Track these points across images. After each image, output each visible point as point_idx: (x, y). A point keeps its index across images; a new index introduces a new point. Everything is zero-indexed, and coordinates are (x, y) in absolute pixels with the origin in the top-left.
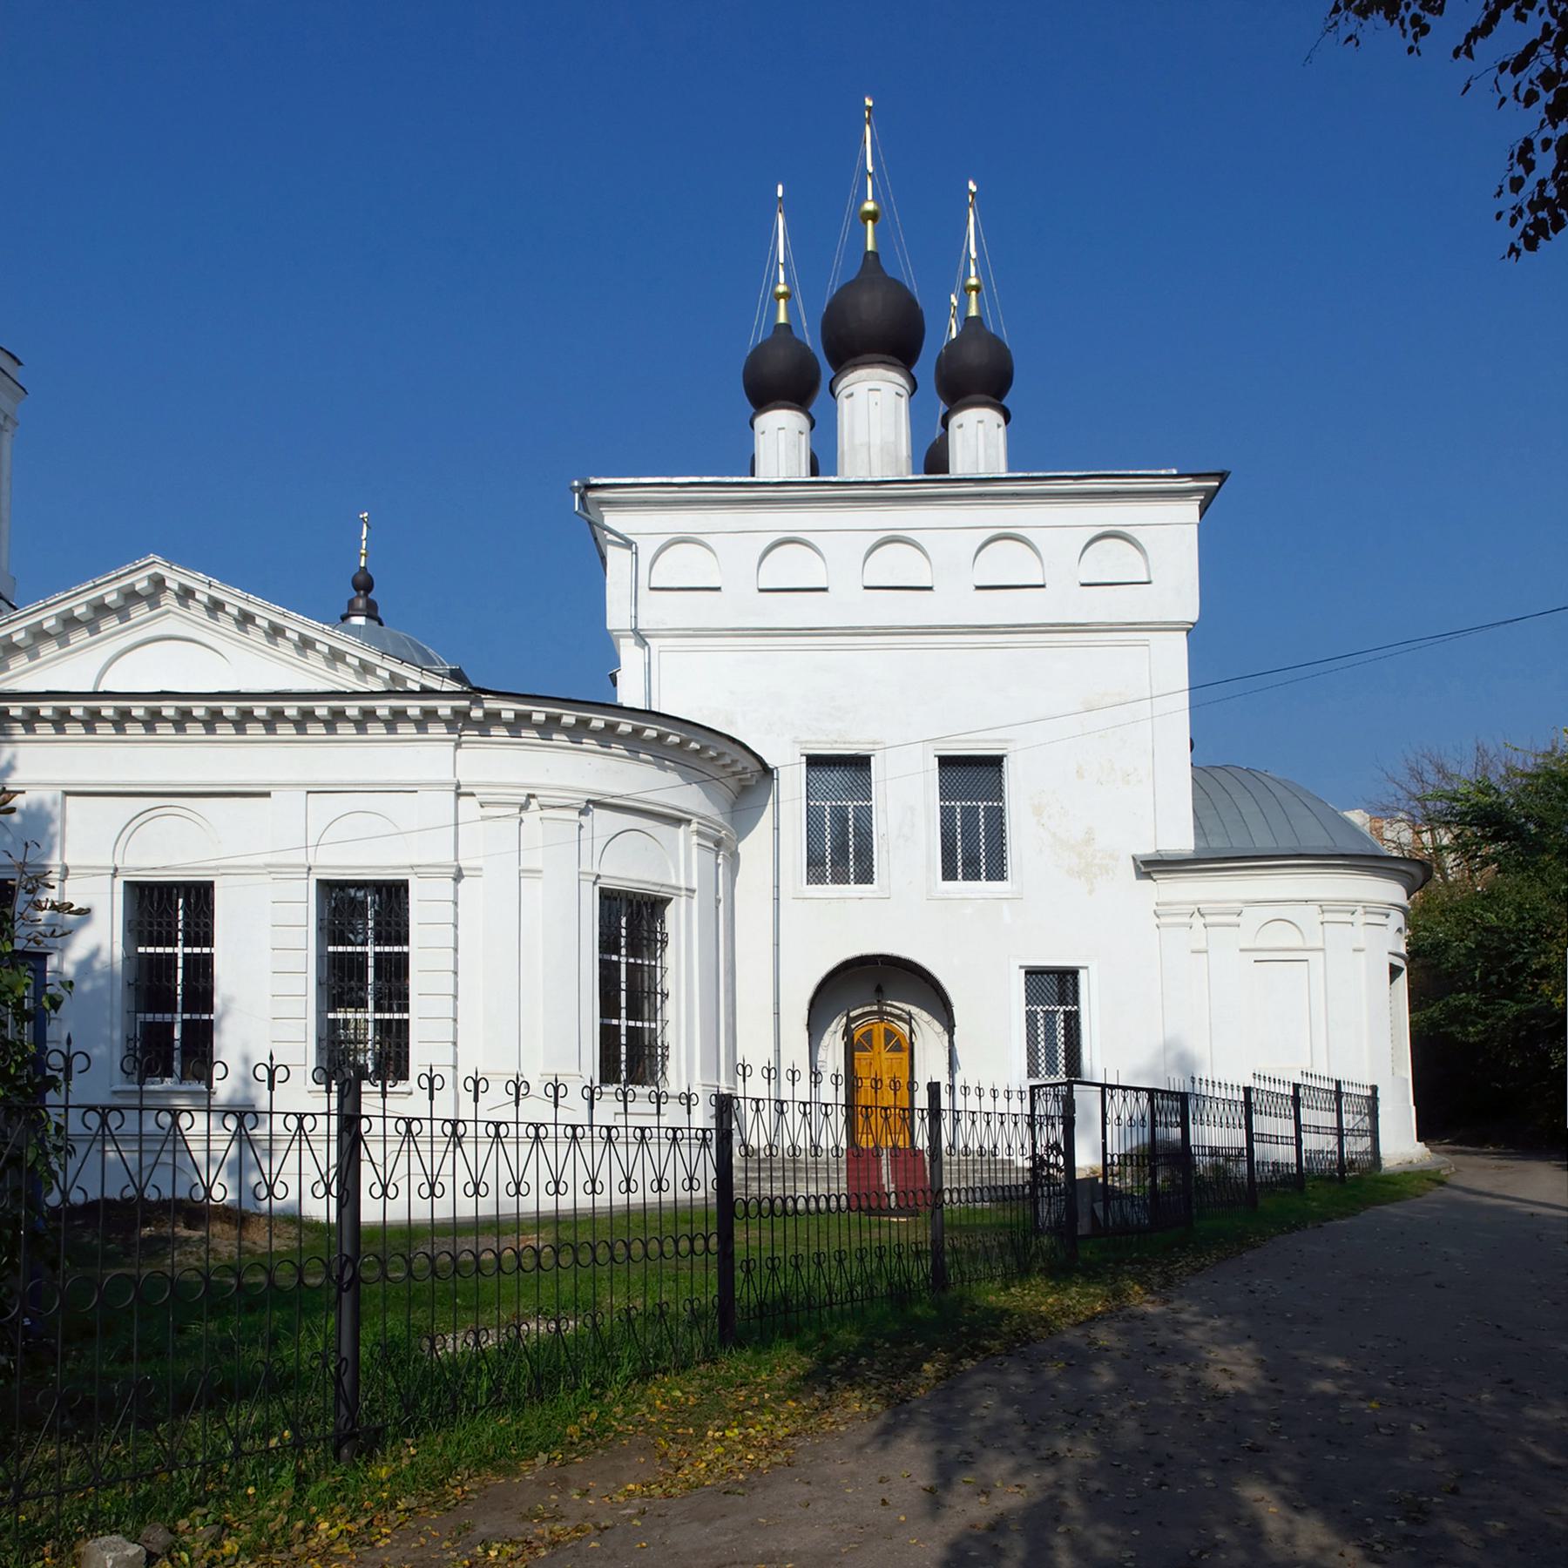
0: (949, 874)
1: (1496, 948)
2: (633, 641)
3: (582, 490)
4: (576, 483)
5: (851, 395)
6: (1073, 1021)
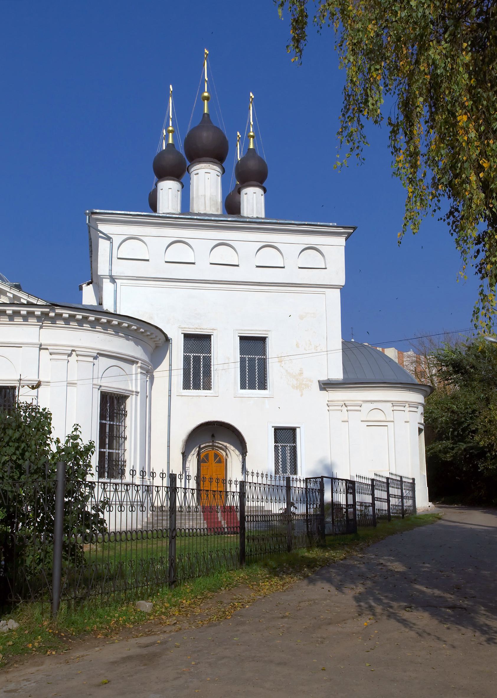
0: (243, 387)
1: (456, 420)
2: (109, 280)
3: (90, 214)
4: (87, 211)
5: (198, 174)
6: (294, 450)
